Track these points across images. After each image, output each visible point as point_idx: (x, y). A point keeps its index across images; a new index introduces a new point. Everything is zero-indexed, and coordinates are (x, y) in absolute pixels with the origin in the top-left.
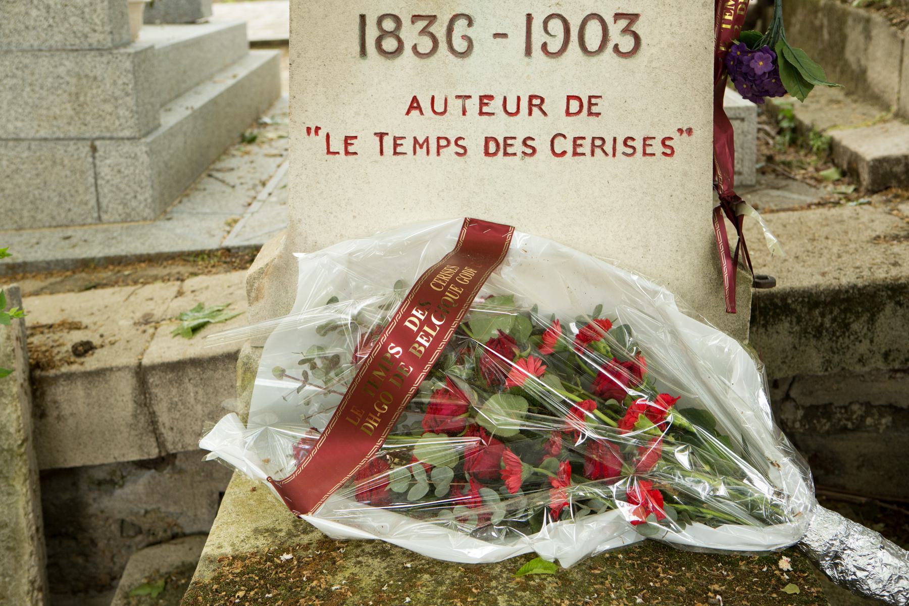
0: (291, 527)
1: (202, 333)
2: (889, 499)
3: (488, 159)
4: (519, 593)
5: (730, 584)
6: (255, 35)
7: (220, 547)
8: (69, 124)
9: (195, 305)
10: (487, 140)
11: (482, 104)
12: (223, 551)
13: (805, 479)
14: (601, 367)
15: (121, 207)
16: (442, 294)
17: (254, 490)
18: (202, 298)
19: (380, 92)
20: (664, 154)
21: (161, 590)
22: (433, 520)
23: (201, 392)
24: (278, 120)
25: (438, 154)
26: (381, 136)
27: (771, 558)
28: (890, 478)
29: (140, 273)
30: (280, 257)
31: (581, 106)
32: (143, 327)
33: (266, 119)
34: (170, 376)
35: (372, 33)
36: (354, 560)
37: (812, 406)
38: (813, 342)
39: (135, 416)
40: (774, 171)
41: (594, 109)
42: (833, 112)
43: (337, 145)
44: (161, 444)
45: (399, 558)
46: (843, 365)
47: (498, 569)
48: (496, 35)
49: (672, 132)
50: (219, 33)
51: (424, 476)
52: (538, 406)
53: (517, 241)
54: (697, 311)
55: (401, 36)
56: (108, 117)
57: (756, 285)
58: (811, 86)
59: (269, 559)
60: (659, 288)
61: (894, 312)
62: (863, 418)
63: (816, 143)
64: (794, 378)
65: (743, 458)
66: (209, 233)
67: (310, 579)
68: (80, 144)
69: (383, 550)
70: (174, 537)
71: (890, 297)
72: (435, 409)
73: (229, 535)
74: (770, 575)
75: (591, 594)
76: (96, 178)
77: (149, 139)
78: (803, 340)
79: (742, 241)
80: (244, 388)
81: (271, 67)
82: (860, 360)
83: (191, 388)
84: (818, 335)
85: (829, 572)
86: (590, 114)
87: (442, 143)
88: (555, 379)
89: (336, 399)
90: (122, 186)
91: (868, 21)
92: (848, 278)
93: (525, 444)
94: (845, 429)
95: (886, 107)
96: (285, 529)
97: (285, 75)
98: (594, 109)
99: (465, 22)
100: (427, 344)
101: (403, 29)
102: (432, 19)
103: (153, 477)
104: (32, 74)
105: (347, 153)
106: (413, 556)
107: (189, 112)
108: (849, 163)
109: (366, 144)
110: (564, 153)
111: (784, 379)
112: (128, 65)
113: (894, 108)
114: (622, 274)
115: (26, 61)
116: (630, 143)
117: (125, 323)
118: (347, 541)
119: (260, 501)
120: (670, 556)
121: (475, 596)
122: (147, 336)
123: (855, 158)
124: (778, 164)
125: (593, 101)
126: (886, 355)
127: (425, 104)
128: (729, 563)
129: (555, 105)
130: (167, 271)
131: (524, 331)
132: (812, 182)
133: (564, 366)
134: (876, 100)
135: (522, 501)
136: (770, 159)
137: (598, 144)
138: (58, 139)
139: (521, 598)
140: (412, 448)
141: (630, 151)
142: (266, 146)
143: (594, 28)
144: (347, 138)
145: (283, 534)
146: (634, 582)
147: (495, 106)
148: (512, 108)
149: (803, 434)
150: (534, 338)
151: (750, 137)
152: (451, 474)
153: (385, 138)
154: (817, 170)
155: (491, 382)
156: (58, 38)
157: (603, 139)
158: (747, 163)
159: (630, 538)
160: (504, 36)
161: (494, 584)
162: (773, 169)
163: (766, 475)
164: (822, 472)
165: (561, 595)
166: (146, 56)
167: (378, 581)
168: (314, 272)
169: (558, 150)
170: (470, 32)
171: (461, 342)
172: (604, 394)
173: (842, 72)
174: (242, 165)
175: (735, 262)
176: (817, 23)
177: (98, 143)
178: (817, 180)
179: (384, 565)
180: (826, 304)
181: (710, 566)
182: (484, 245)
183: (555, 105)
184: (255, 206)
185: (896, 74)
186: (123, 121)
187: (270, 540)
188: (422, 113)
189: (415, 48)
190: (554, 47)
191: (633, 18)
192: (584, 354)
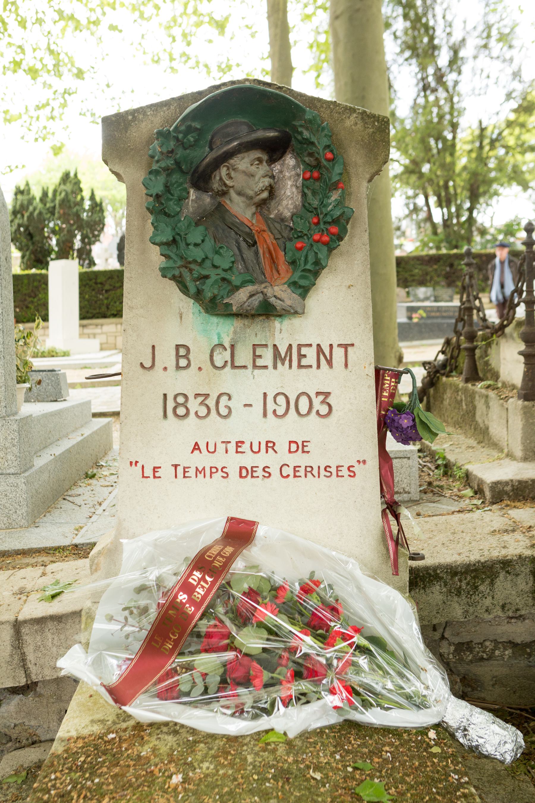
0: (115, 718)
1: (58, 599)
2: (514, 706)
4: (261, 754)
5: (397, 747)
6: (96, 409)
7: (68, 732)
9: (54, 581)
10: (241, 468)
11: (237, 446)
12: (70, 734)
13: (443, 679)
14: (315, 611)
15: (6, 519)
16: (213, 562)
17: (91, 696)
18: (58, 576)
19: (174, 440)
20: (350, 476)
21: (24, 778)
22: (206, 707)
23: (56, 638)
24: (110, 463)
25: (211, 477)
26: (176, 466)
27: (423, 731)
28: (514, 692)
29: (17, 562)
30: (112, 543)
31: (298, 447)
32: (19, 596)
33: (102, 463)
34: (36, 627)
35: (171, 404)
36: (155, 737)
37: (459, 643)
38: (456, 599)
39: (11, 656)
40: (432, 491)
41: (306, 449)
42: (469, 454)
43: (149, 472)
44: (28, 676)
45: (184, 735)
46: (476, 614)
47: (248, 739)
48: (245, 405)
50: (73, 407)
51: (201, 679)
52: (273, 632)
53: (261, 531)
54: (375, 575)
55: (188, 406)
57: (412, 558)
58: (436, 435)
59: (100, 738)
60: (348, 559)
61: (506, 578)
62: (493, 651)
63: (459, 474)
64: (446, 622)
65: (405, 666)
66: (63, 535)
67: (127, 749)
69: (174, 728)
70: (33, 743)
71: (502, 568)
72: (209, 635)
73: (75, 724)
74: (422, 742)
75: (307, 754)
77: (26, 474)
78: (449, 597)
79: (401, 529)
80: (86, 629)
81: (106, 430)
82: (487, 611)
83: (50, 636)
84: (459, 594)
85: (461, 740)
86: (303, 452)
87: (213, 470)
88: (285, 617)
89: (144, 633)
90: (7, 505)
91: (487, 396)
92: (474, 557)
93: (267, 659)
94: (482, 659)
95: (501, 450)
96: (111, 720)
97: (116, 435)
98: (306, 449)
99: (227, 398)
100: (203, 593)
101: (189, 402)
102: (207, 396)
103: (21, 700)
105: (155, 477)
106: (193, 731)
107: (53, 457)
108: (478, 486)
109: (166, 472)
110: (288, 476)
111: (440, 624)
112: (15, 427)
113: (506, 451)
114: (326, 551)
116: (328, 469)
117: (7, 594)
118: (151, 725)
119: (95, 703)
120: (359, 731)
121: (232, 755)
122: (21, 601)
123: (481, 482)
124: (435, 487)
125: (305, 444)
126: (503, 607)
127: (203, 447)
128: (397, 735)
129: (282, 446)
130: (35, 560)
131: (266, 588)
132: (456, 498)
133: (292, 610)
134: (495, 445)
135: (263, 694)
136: (430, 484)
137: (309, 470)
139: (262, 756)
140: (194, 660)
141: (329, 474)
142: (102, 480)
144: (155, 468)
145: (109, 723)
146: (335, 747)
147: (246, 447)
148: (256, 449)
149: (455, 662)
150: (273, 592)
151: (414, 469)
152: (218, 679)
153: (178, 468)
154: (459, 490)
155: (243, 619)
157: (311, 467)
158: (413, 486)
159: (334, 719)
160: (250, 405)
161: (245, 748)
162: (431, 490)
163: (419, 678)
164: (470, 689)
165: (288, 754)
166: (27, 420)
167: (171, 749)
168: (132, 550)
169: (284, 474)
170: (230, 404)
171: (224, 592)
172: (316, 627)
173: (475, 429)
174: (85, 492)
175: (397, 543)
176: (459, 398)
178: (458, 496)
179: (175, 739)
180: (462, 573)
181: (384, 736)
182: (240, 534)
183: (282, 446)
184: (94, 518)
185: (505, 429)
186: (10, 462)
187: (101, 726)
188: (201, 452)
189: (196, 413)
190: (280, 412)
192: (304, 601)
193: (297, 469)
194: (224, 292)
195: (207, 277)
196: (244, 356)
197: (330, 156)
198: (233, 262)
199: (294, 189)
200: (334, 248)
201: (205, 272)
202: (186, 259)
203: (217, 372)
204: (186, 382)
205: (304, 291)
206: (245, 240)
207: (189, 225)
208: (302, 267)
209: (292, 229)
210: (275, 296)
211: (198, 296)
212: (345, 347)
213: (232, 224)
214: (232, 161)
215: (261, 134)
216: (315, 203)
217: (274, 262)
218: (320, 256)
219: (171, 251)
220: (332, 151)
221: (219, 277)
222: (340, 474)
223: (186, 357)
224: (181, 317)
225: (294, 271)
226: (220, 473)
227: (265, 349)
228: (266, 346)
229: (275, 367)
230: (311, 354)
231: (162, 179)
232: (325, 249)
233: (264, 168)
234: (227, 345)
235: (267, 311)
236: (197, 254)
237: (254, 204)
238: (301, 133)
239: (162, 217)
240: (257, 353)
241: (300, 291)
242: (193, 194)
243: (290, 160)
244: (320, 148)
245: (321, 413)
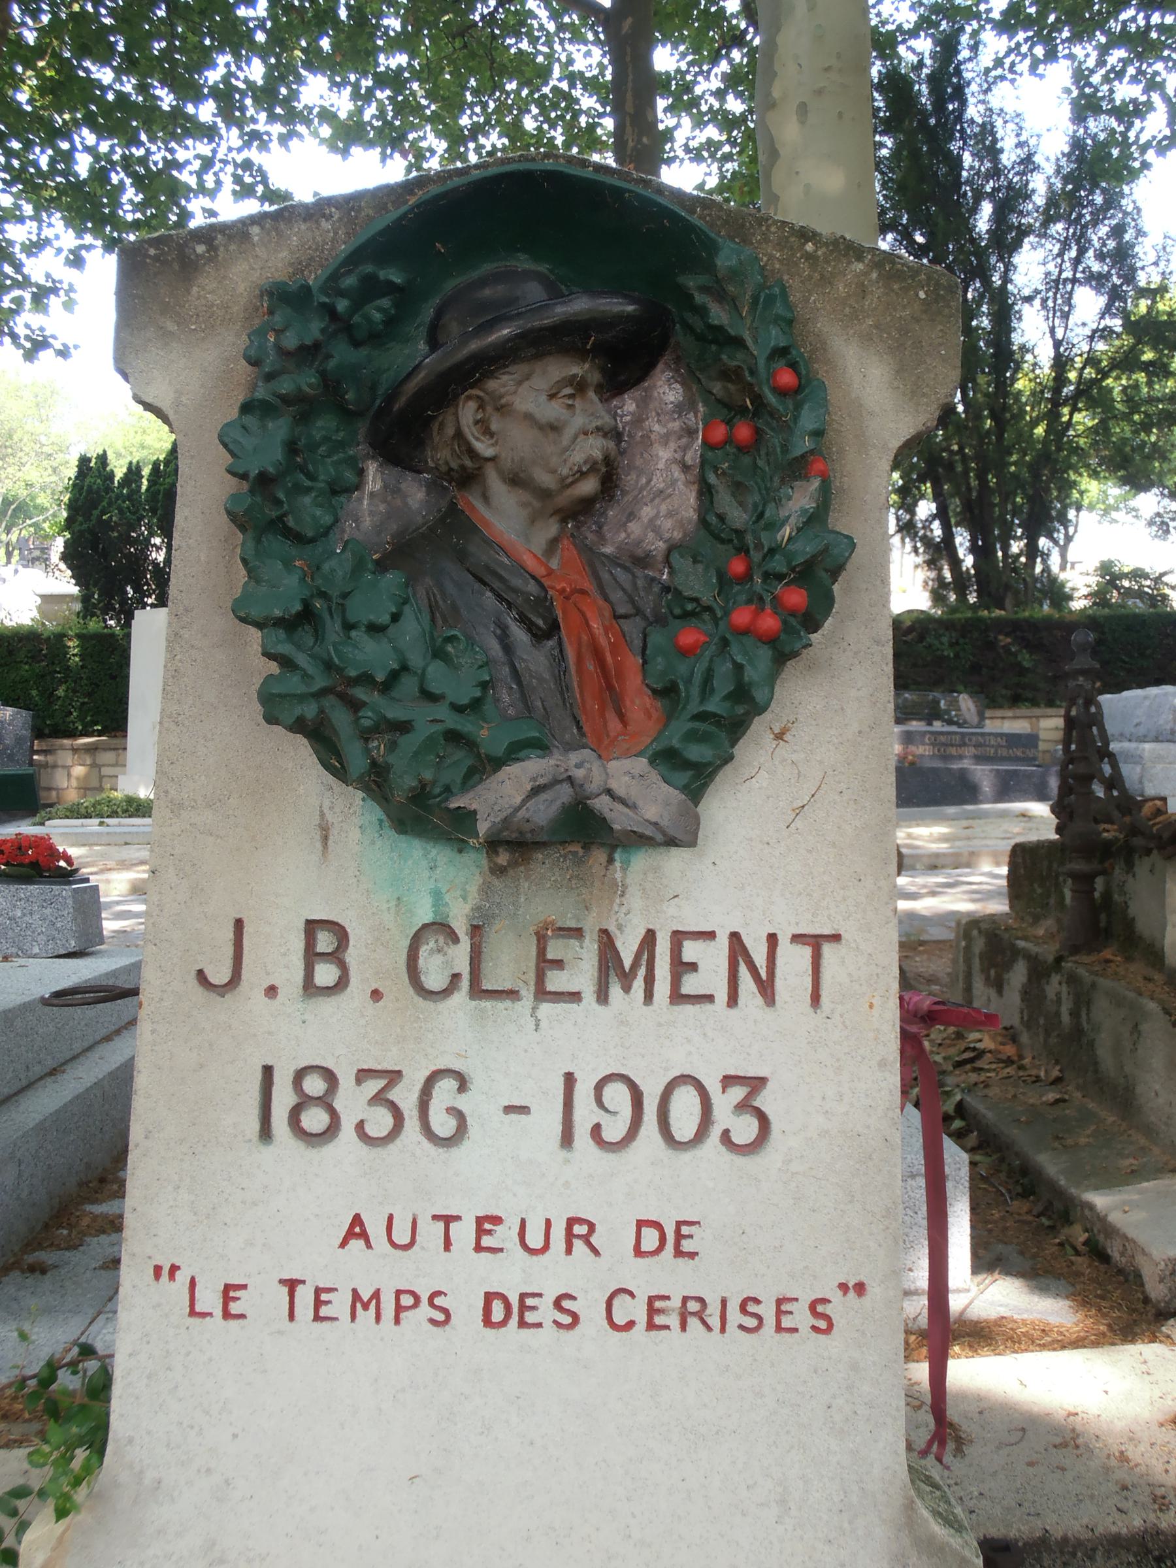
10: (489, 1297)
11: (480, 1232)
20: (815, 1329)
25: (397, 1321)
26: (292, 1285)
41: (687, 1246)
43: (209, 1299)
48: (509, 1109)
55: (338, 1105)
86: (679, 1253)
98: (687, 1246)
102: (394, 1077)
105: (227, 1315)
109: (263, 1300)
110: (631, 1324)
116: (751, 1308)
125: (685, 1230)
127: (376, 1229)
129: (615, 1236)
137: (692, 1311)
141: (751, 1323)
144: (228, 1288)
147: (505, 1236)
148: (535, 1239)
153: (300, 1289)
157: (701, 1300)
160: (523, 1110)
169: (619, 1320)
170: (463, 1103)
183: (615, 1236)
188: (369, 1245)
189: (360, 1127)
191: (756, 1084)
193: (658, 1304)
194: (454, 776)
195: (404, 727)
196: (509, 962)
197: (787, 378)
198: (484, 685)
199: (677, 473)
200: (795, 655)
201: (395, 713)
202: (340, 670)
203: (428, 1005)
204: (337, 1034)
205: (694, 771)
206: (523, 619)
207: (358, 567)
208: (694, 707)
209: (666, 589)
210: (609, 792)
211: (376, 782)
212: (815, 942)
213: (487, 567)
214: (492, 384)
215: (580, 305)
216: (738, 517)
217: (610, 687)
218: (750, 674)
219: (299, 647)
220: (793, 366)
221: (439, 727)
222: (786, 1322)
223: (337, 957)
224: (325, 838)
225: (670, 716)
226: (425, 1311)
227: (574, 943)
228: (577, 933)
229: (603, 996)
230: (711, 962)
231: (279, 428)
232: (764, 654)
233: (587, 413)
234: (460, 927)
235: (585, 830)
236: (372, 655)
237: (556, 512)
238: (702, 311)
239: (276, 543)
240: (550, 956)
241: (684, 777)
242: (374, 476)
243: (667, 390)
244: (760, 353)
245: (737, 1139)
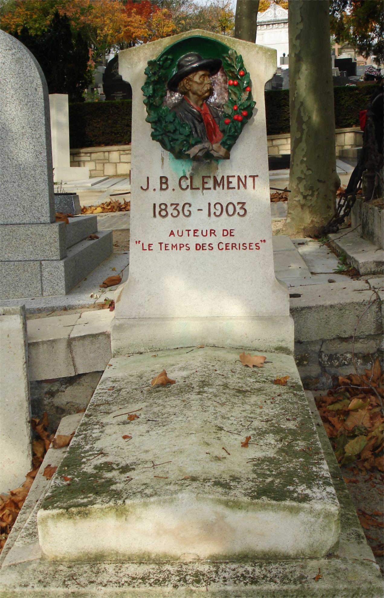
3: (197, 251)
8: (31, 254)
10: (197, 245)
11: (194, 233)
15: (51, 289)
26: (161, 244)
43: (146, 247)
48: (199, 210)
49: (259, 241)
56: (47, 251)
68: (35, 262)
76: (41, 277)
86: (231, 235)
87: (181, 246)
94: (344, 364)
98: (232, 234)
102: (178, 205)
104: (17, 234)
105: (149, 249)
110: (222, 249)
115: (14, 229)
127: (175, 233)
129: (219, 232)
137: (234, 246)
138: (26, 261)
141: (245, 248)
143: (231, 208)
144: (149, 245)
147: (199, 233)
148: (204, 234)
156: (28, 219)
160: (201, 210)
169: (220, 248)
177: (43, 262)
183: (219, 232)
189: (172, 214)
191: (244, 204)
